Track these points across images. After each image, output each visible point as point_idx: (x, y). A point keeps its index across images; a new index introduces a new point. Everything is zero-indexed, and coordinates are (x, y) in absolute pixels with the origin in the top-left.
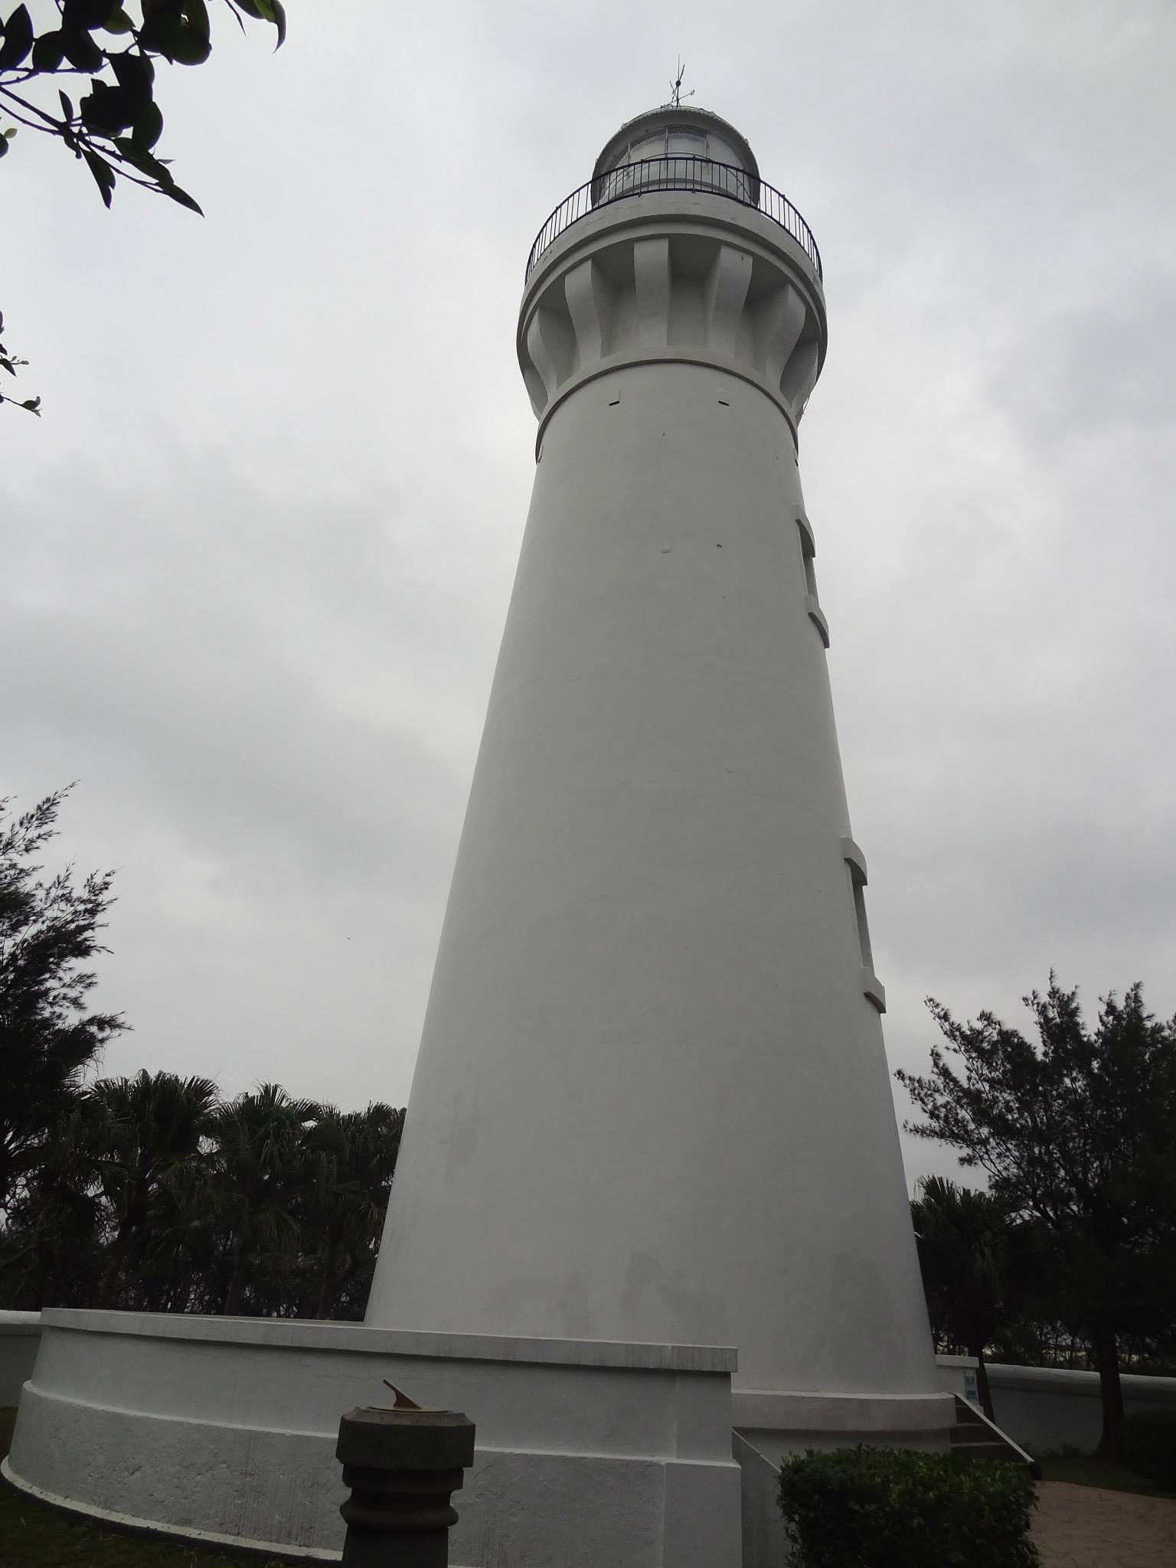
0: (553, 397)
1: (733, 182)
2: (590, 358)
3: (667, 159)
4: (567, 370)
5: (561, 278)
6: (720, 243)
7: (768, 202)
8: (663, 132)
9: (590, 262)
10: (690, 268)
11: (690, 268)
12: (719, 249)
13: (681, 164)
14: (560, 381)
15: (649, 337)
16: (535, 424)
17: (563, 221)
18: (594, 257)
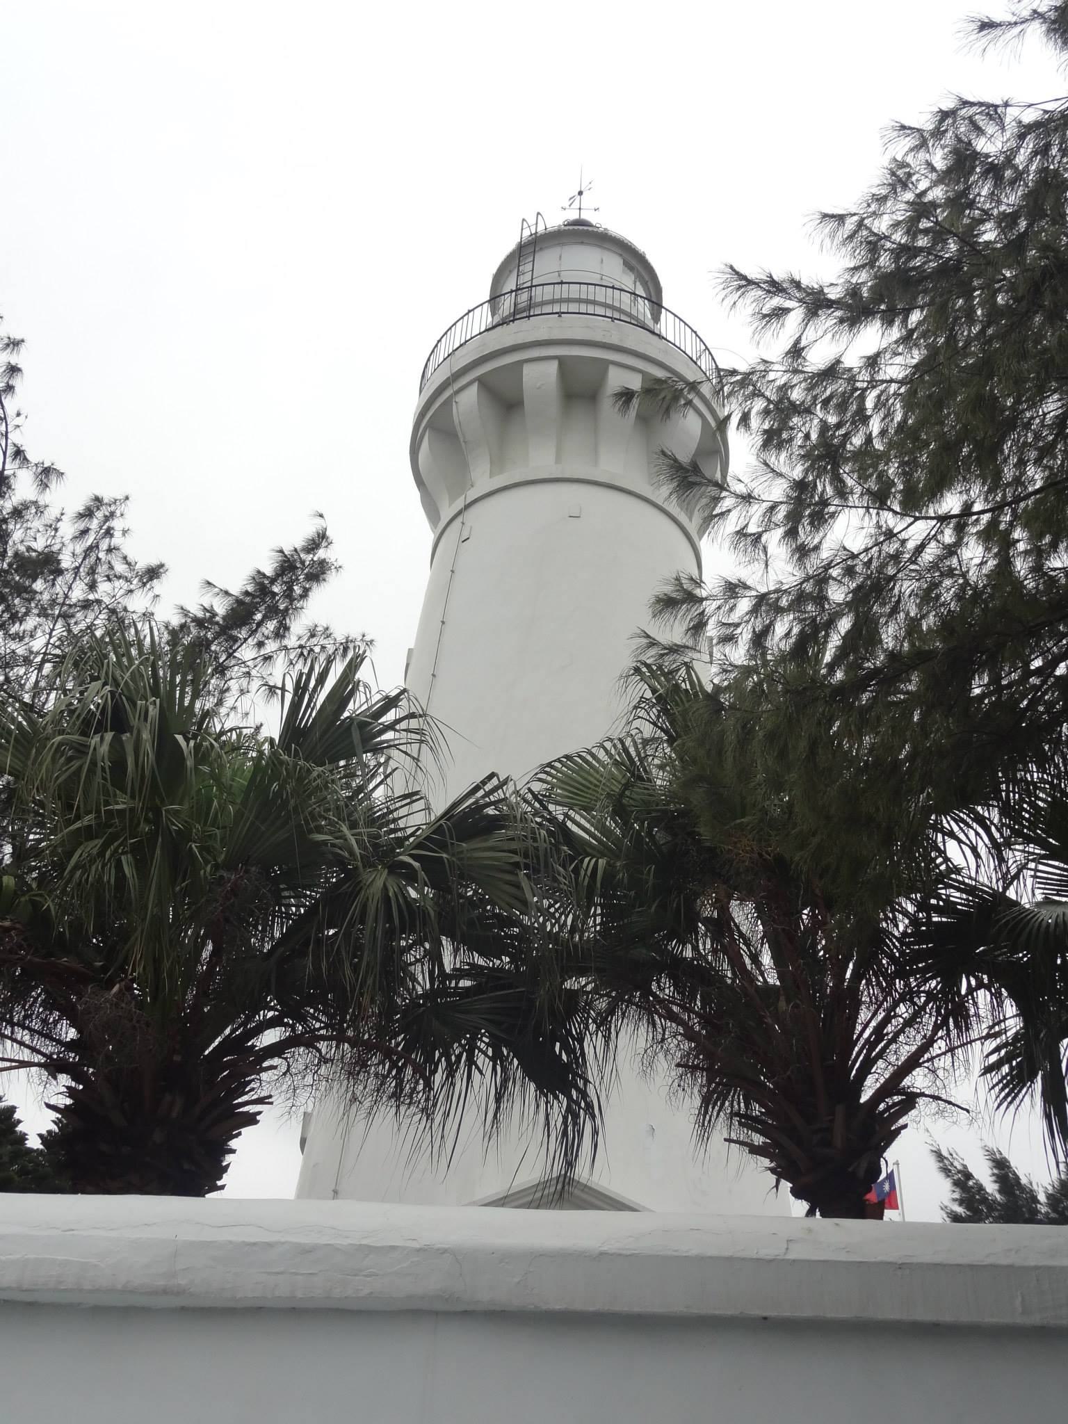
0: (446, 513)
1: (643, 309)
2: (483, 480)
3: (562, 283)
4: (498, 464)
5: (448, 402)
6: (606, 363)
7: (667, 326)
8: (859, 318)
9: (476, 384)
10: (580, 389)
11: (580, 389)
12: (606, 371)
13: (548, 289)
14: (452, 499)
15: (540, 457)
16: (430, 537)
17: (457, 339)
18: (480, 380)
